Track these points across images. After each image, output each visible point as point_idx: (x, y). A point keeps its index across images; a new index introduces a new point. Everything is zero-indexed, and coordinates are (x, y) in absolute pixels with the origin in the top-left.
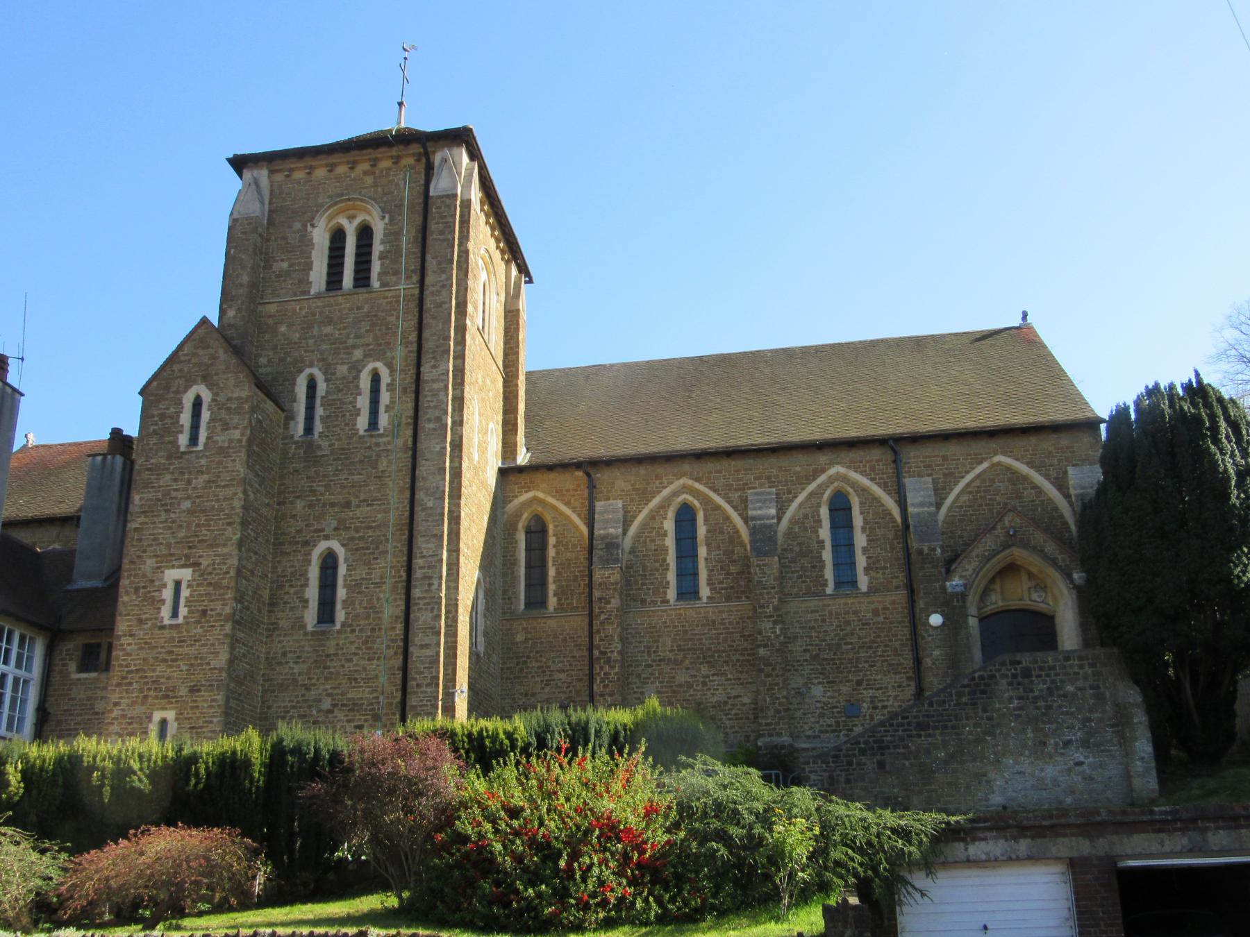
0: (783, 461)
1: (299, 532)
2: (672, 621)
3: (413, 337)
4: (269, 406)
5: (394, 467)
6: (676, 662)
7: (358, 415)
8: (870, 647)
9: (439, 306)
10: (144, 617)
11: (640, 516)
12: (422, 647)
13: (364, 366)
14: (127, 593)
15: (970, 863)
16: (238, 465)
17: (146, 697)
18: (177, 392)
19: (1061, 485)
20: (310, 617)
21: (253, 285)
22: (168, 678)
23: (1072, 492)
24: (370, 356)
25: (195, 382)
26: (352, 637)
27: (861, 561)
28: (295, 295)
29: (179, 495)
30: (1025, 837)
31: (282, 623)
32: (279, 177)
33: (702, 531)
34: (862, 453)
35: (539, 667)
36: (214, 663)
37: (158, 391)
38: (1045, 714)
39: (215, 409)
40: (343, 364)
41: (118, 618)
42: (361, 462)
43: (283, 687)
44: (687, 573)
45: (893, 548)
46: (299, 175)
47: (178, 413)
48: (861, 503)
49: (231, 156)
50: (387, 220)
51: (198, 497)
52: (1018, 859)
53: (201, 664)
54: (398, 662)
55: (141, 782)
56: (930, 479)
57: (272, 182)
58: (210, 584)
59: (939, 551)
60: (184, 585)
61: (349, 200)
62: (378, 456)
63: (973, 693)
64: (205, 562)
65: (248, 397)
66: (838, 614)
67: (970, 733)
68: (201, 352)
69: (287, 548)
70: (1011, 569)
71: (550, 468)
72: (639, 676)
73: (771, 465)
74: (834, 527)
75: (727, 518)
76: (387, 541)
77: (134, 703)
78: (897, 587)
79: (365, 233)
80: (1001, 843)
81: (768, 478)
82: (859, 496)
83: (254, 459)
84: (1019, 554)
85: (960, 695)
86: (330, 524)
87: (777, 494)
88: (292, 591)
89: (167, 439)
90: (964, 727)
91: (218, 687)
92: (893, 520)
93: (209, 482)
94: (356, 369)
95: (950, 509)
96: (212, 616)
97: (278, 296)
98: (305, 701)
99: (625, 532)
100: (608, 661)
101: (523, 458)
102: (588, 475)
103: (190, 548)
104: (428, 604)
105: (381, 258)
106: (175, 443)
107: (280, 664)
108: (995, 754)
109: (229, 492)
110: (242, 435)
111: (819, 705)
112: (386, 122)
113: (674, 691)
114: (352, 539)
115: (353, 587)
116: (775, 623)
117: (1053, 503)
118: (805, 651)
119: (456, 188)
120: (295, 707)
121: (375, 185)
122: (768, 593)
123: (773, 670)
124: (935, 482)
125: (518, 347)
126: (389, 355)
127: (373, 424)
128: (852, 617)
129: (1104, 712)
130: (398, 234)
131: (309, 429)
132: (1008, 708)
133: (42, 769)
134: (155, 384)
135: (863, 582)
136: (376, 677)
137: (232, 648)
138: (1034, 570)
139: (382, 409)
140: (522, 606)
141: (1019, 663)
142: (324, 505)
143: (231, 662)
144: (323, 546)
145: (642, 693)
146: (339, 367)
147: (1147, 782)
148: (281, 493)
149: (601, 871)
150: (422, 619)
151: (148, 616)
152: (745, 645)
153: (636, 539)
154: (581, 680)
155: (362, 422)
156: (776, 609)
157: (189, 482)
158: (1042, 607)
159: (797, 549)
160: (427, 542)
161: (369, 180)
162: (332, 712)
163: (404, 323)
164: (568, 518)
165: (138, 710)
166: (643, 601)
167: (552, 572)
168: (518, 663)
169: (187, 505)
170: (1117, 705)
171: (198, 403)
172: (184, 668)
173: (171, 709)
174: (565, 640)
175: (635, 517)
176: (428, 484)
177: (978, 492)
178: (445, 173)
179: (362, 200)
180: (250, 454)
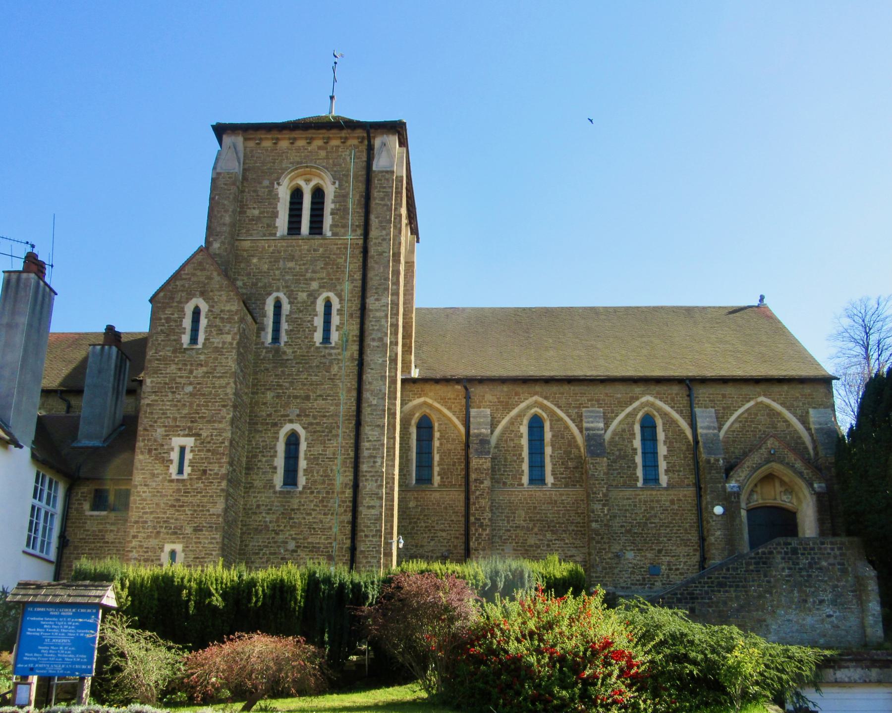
0: (609, 389)
1: (270, 415)
2: (525, 499)
3: (358, 276)
4: (249, 318)
5: (343, 372)
6: (528, 529)
7: (315, 331)
8: (668, 527)
9: (381, 254)
10: (156, 472)
11: (505, 422)
12: (369, 507)
13: (319, 295)
14: (142, 453)
15: (837, 683)
16: (231, 362)
17: (158, 533)
18: (180, 302)
19: (804, 421)
20: (278, 479)
21: (233, 225)
22: (176, 520)
23: (812, 426)
24: (324, 287)
25: (194, 296)
26: (311, 497)
27: (663, 465)
28: (265, 235)
29: (183, 381)
30: (876, 667)
31: (256, 483)
32: (251, 144)
33: (548, 435)
34: (665, 388)
35: (426, 527)
36: (212, 511)
37: (164, 300)
38: (807, 581)
39: (211, 318)
40: (303, 291)
41: (135, 471)
42: (317, 366)
43: (257, 531)
44: (537, 466)
45: (685, 457)
46: (267, 144)
47: (181, 318)
48: (664, 424)
49: (214, 124)
50: (337, 185)
51: (199, 384)
52: (870, 682)
53: (203, 511)
54: (349, 517)
55: (217, 601)
56: (713, 410)
57: (245, 148)
58: (209, 451)
59: (721, 462)
60: (187, 450)
61: (307, 167)
62: (331, 363)
63: (757, 563)
64: (204, 434)
65: (237, 310)
66: (645, 501)
67: (755, 591)
68: (199, 273)
69: (260, 427)
70: (769, 478)
71: (437, 381)
72: (500, 537)
73: (600, 391)
74: (643, 440)
75: (567, 427)
76: (338, 427)
77: (149, 537)
78: (688, 485)
79: (318, 194)
80: (859, 671)
81: (598, 401)
82: (662, 418)
83: (241, 358)
84: (776, 467)
85: (748, 564)
86: (294, 411)
87: (604, 413)
88: (264, 459)
89: (172, 338)
90: (751, 586)
91: (216, 528)
92: (686, 437)
93: (207, 373)
94: (313, 296)
95: (726, 433)
96: (210, 475)
97: (251, 235)
98: (275, 542)
99: (492, 432)
100: (481, 525)
101: (415, 373)
102: (466, 389)
103: (192, 422)
104: (373, 476)
105: (332, 214)
106: (178, 341)
107: (255, 513)
108: (772, 606)
109: (223, 382)
110: (233, 339)
111: (630, 565)
112: (319, 109)
113: (526, 550)
114: (311, 424)
115: (312, 460)
116: (604, 505)
117: (798, 433)
118: (622, 526)
119: (392, 166)
120: (267, 547)
121: (327, 158)
122: (599, 484)
123: (602, 538)
124: (717, 412)
125: (412, 289)
126: (338, 287)
127: (326, 339)
128: (655, 504)
129: (847, 581)
130: (345, 196)
131: (276, 338)
132: (782, 575)
133: (142, 585)
134: (162, 294)
135: (664, 480)
136: (330, 528)
137: (227, 500)
138: (786, 479)
139: (333, 328)
140: (414, 482)
141: (790, 544)
142: (289, 397)
143: (226, 510)
144: (287, 428)
145: (503, 550)
146: (300, 294)
147: (876, 631)
148: (254, 385)
149: (613, 684)
150: (368, 487)
151: (159, 471)
152: (579, 520)
153: (500, 439)
154: (457, 538)
155: (318, 337)
156: (605, 495)
157: (191, 372)
158: (789, 506)
159: (617, 453)
160: (372, 430)
161: (323, 153)
162: (296, 551)
163: (351, 265)
164: (449, 419)
165: (153, 542)
166: (505, 484)
167: (437, 458)
168: (410, 523)
169: (189, 389)
170: (856, 577)
171: (197, 313)
172: (189, 513)
173: (179, 543)
174: (446, 508)
175: (499, 422)
176: (372, 387)
177: (746, 422)
178: (384, 154)
179: (317, 168)
180: (239, 354)
